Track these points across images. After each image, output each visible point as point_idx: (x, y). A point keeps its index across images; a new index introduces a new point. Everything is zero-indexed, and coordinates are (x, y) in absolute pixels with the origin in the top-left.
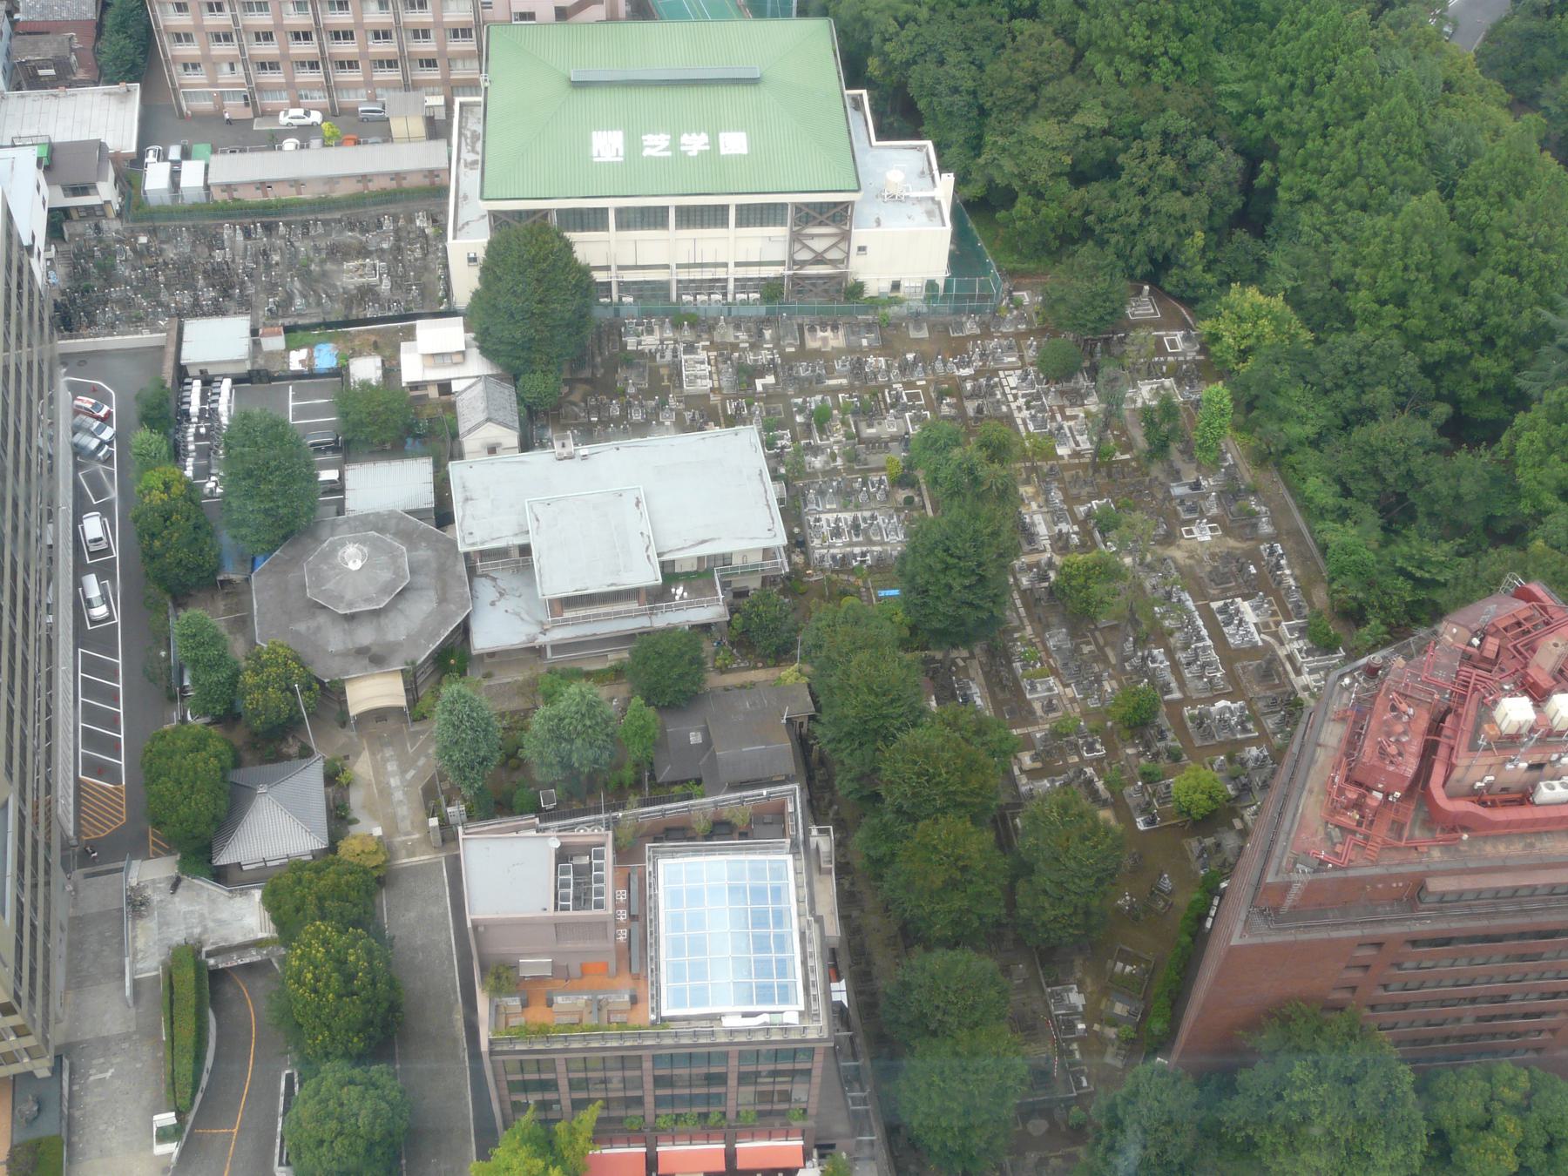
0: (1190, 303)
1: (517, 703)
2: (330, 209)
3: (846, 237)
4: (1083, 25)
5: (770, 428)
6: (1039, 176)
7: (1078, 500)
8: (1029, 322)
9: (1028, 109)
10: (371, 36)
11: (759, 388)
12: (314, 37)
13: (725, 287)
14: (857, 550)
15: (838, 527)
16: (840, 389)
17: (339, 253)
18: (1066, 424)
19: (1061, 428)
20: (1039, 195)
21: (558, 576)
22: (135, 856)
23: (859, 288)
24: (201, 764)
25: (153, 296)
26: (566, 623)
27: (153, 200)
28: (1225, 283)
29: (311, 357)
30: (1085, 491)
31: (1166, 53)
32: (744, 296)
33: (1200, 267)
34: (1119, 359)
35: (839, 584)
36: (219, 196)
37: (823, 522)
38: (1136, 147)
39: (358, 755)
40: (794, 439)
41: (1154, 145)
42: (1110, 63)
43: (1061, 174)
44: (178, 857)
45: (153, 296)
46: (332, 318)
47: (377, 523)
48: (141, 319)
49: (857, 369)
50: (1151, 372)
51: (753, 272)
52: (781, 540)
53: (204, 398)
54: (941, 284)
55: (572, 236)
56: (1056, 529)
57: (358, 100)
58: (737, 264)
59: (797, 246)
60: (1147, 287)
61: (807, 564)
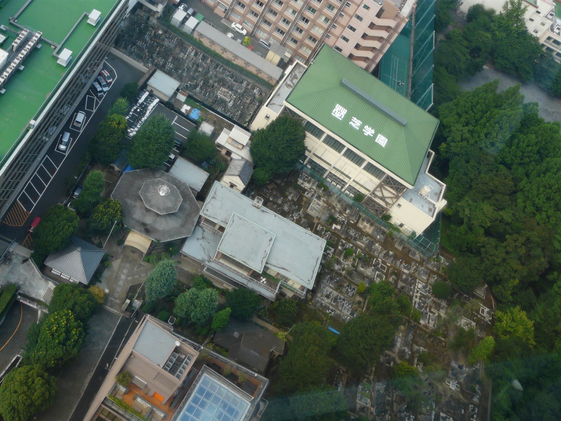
0: (498, 301)
1: (184, 280)
2: (229, 66)
3: (397, 197)
4: (524, 182)
5: (330, 244)
6: (475, 223)
7: (417, 343)
8: (438, 269)
9: (486, 197)
10: (282, 19)
11: (333, 228)
12: (264, 6)
13: (344, 185)
14: (331, 307)
15: (330, 295)
16: (360, 247)
17: (222, 82)
18: (429, 313)
19: (427, 314)
20: (471, 229)
21: (227, 246)
22: (16, 241)
23: (388, 217)
24: (67, 227)
25: (151, 53)
26: (218, 263)
27: (173, 22)
28: (514, 304)
29: (190, 111)
30: (421, 341)
31: (547, 211)
32: (348, 193)
33: (510, 292)
34: (463, 304)
35: (318, 315)
36: (196, 36)
37: (326, 290)
38: (515, 236)
39: (117, 259)
40: (334, 253)
41: (522, 240)
42: (524, 202)
43: (483, 227)
44: (32, 252)
45: (151, 53)
46: (206, 103)
47: (176, 184)
48: (142, 58)
49: (371, 244)
50: (471, 317)
51: (357, 187)
52: (311, 287)
53: (146, 99)
54: (417, 235)
55: (308, 134)
56: (403, 348)
57: (262, 36)
58: (354, 181)
59: (379, 189)
60: (486, 286)
61: (311, 300)
